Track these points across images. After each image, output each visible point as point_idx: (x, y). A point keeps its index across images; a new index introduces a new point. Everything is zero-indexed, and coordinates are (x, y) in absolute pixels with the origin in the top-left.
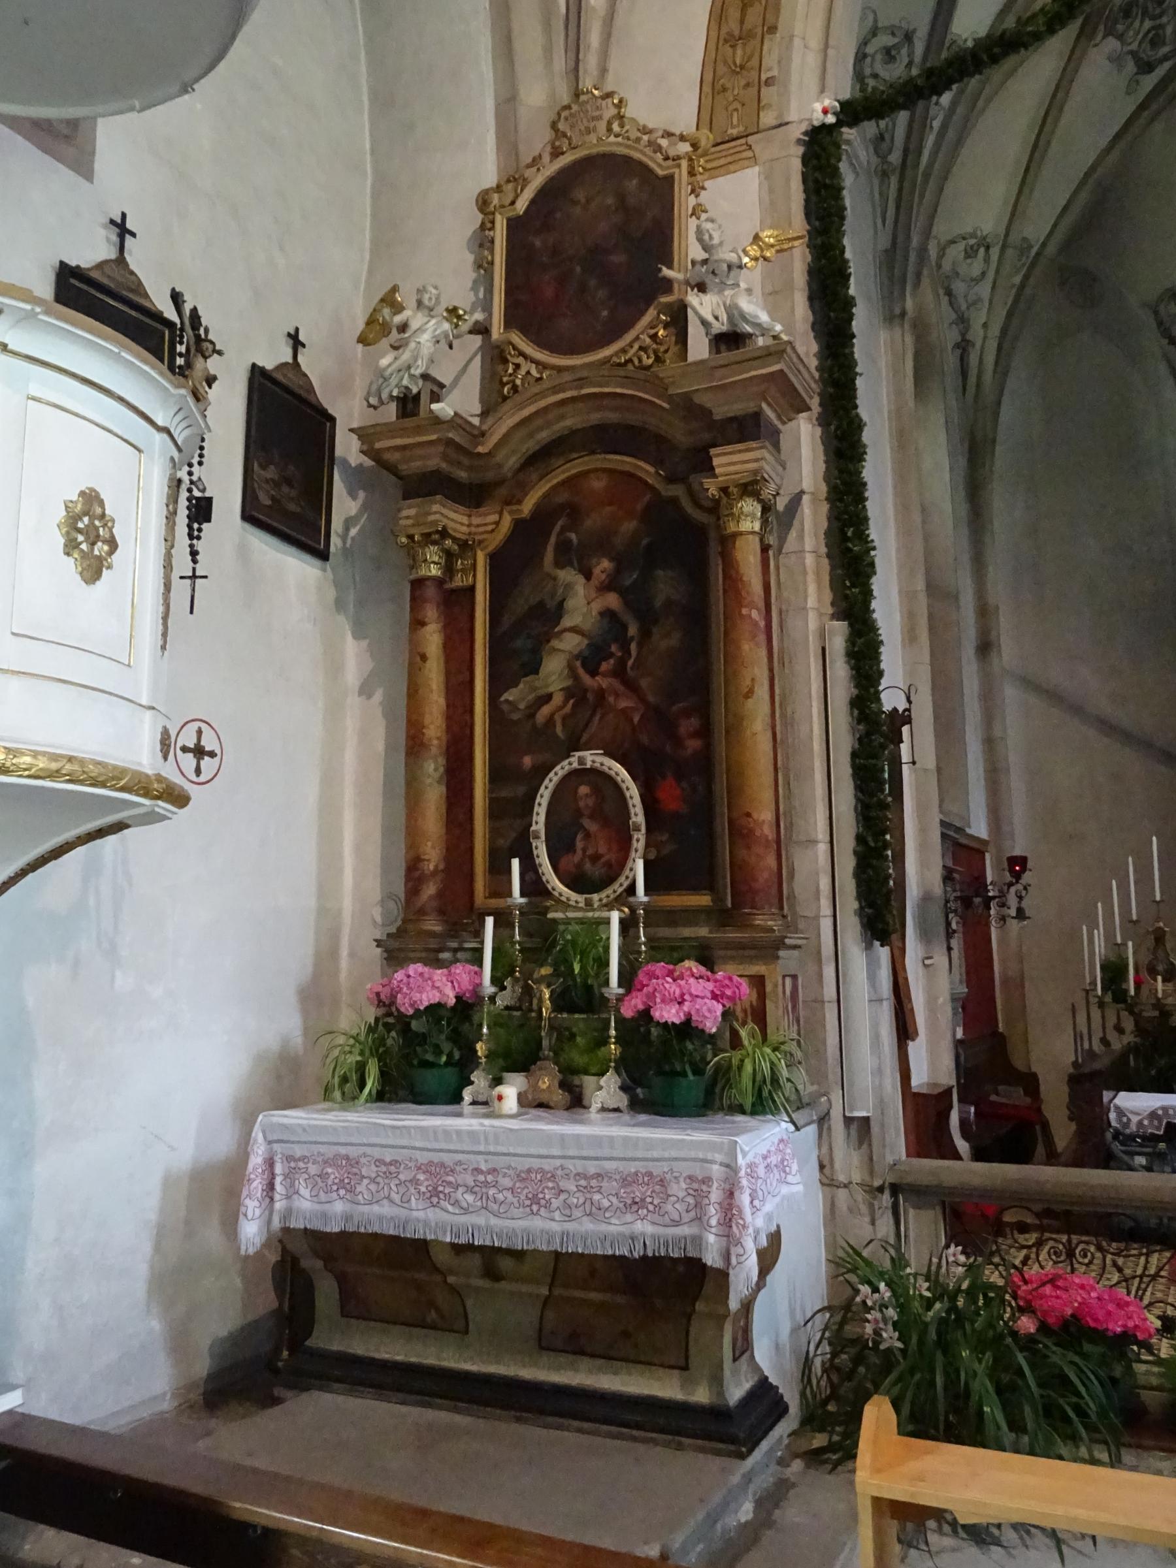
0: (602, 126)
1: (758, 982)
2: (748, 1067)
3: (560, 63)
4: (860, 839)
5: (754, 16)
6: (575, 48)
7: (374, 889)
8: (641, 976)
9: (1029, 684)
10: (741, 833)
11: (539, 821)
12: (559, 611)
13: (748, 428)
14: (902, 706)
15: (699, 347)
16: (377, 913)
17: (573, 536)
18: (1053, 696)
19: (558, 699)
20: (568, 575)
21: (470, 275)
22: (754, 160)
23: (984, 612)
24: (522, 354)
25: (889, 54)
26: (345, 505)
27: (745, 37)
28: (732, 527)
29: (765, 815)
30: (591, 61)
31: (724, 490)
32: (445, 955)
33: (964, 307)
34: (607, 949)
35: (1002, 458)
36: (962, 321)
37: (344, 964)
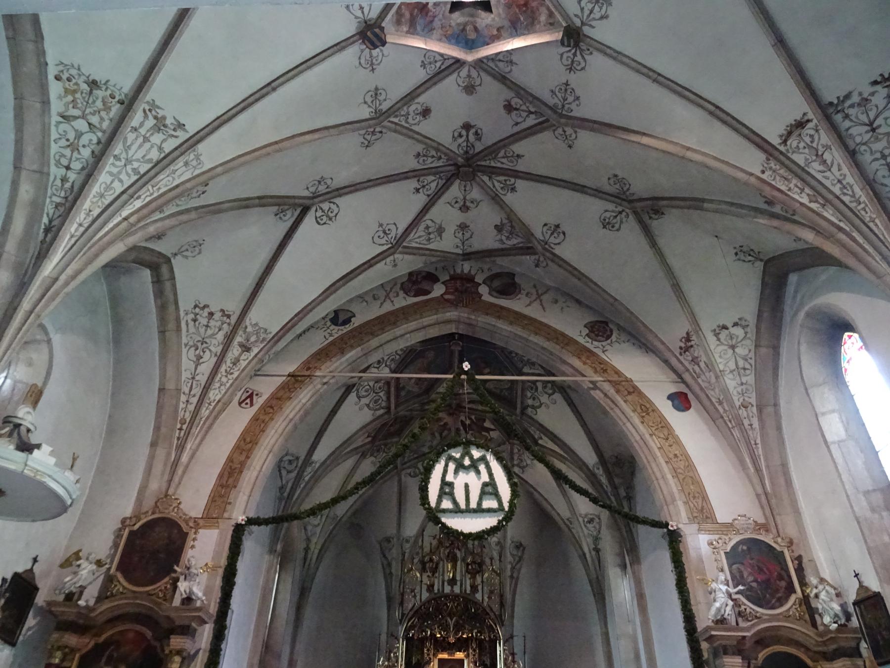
0: (171, 508)
3: (166, 477)
5: (231, 481)
13: (187, 631)
15: (177, 602)
17: (115, 655)
21: (110, 543)
22: (218, 527)
24: (119, 581)
25: (290, 462)
26: (31, 621)
30: (173, 485)
33: (310, 534)
36: (308, 540)
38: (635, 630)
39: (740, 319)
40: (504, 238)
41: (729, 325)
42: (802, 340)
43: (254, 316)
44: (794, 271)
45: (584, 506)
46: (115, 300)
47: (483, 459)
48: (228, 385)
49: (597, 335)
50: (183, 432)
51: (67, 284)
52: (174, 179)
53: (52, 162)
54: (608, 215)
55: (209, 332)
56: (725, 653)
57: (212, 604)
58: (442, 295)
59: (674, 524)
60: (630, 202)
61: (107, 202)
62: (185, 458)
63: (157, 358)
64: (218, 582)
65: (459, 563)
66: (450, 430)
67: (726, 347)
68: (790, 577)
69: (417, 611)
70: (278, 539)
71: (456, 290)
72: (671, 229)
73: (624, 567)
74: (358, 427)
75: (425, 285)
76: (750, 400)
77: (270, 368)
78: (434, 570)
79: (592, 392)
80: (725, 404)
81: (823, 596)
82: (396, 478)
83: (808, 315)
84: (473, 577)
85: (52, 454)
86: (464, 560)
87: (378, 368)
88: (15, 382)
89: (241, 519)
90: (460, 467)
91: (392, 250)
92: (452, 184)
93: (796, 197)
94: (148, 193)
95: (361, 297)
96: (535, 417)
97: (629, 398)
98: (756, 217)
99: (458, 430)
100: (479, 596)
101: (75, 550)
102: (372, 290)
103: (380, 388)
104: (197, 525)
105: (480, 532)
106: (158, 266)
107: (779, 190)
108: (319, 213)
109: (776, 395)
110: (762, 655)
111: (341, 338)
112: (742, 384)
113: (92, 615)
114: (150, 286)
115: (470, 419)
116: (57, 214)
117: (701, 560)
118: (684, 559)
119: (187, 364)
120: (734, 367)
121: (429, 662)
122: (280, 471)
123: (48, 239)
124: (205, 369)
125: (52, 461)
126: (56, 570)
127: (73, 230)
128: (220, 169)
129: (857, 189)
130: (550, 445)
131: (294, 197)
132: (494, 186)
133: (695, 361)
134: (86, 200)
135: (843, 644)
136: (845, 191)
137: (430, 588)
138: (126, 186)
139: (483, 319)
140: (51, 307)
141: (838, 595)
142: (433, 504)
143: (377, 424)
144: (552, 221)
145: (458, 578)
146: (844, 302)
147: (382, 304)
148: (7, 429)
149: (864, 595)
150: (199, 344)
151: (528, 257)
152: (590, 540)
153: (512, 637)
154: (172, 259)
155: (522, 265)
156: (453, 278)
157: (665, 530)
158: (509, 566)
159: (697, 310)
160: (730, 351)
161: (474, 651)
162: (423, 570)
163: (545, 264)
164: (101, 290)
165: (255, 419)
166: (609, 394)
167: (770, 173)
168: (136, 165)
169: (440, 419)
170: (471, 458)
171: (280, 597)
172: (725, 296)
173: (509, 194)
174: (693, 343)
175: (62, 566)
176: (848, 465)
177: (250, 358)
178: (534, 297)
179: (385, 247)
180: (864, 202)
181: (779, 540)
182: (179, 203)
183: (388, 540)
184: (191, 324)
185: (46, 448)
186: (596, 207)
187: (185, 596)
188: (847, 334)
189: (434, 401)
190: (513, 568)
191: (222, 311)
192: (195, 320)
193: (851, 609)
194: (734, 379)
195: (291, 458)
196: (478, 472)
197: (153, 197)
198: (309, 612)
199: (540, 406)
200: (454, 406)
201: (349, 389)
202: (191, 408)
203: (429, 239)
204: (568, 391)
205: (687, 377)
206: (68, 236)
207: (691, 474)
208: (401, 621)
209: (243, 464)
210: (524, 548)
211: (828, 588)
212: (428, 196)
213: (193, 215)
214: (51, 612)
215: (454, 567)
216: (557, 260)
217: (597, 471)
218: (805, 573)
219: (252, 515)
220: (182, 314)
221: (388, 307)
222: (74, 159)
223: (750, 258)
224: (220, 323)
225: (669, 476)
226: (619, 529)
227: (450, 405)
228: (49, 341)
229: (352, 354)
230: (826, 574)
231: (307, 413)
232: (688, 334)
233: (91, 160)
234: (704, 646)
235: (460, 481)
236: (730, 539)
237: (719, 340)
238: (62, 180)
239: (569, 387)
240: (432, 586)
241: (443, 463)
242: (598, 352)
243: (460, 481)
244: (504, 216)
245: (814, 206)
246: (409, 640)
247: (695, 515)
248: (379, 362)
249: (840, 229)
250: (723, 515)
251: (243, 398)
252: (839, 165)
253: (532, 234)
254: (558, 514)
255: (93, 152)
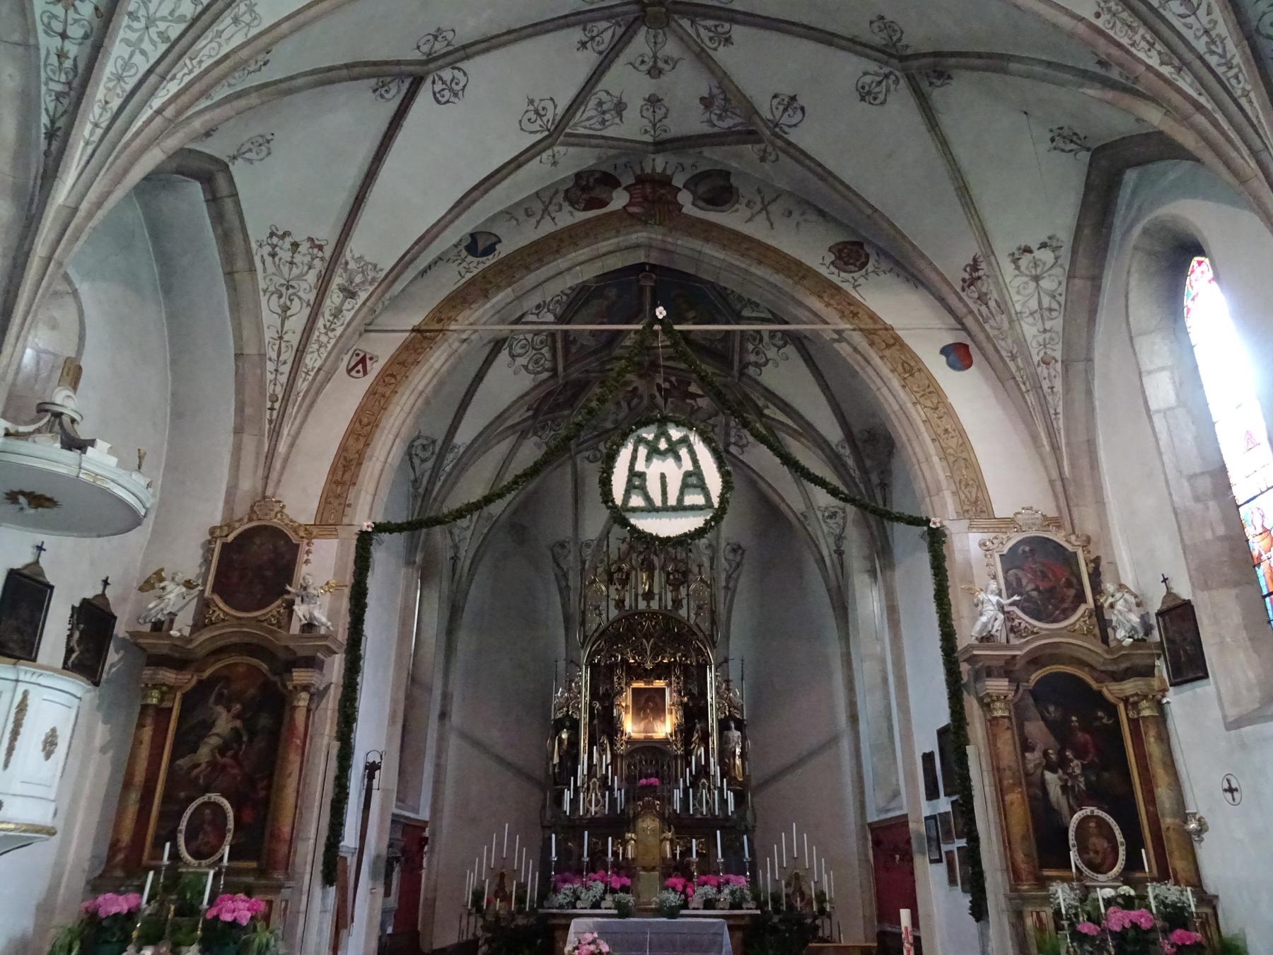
0: (273, 514)
1: (270, 903)
2: (257, 941)
3: (260, 472)
4: (328, 838)
5: (347, 476)
6: (269, 468)
7: (87, 852)
8: (218, 900)
9: (463, 735)
10: (275, 836)
11: (183, 825)
12: (213, 724)
13: (311, 663)
14: (378, 760)
15: (295, 628)
16: (86, 865)
17: (225, 691)
18: (476, 744)
19: (204, 766)
20: (220, 709)
21: (200, 560)
22: (337, 536)
23: (446, 696)
25: (424, 447)
26: (113, 656)
27: (342, 483)
28: (295, 703)
29: (286, 829)
31: (295, 687)
32: (123, 889)
34: (205, 886)
35: (467, 617)
37: (62, 891)
38: (883, 649)
39: (1050, 238)
40: (714, 117)
41: (1034, 247)
42: (1133, 269)
43: (357, 246)
44: (1129, 166)
45: (822, 498)
46: (157, 231)
47: (684, 441)
48: (330, 346)
49: (846, 263)
50: (275, 413)
51: (90, 215)
52: (220, 45)
53: (40, 28)
54: (868, 79)
55: (295, 271)
56: (989, 675)
57: (341, 630)
58: (624, 207)
59: (938, 520)
60: (903, 59)
61: (128, 88)
62: (282, 448)
63: (227, 313)
64: (345, 604)
65: (657, 572)
66: (641, 397)
67: (1026, 279)
68: (1081, 584)
69: (603, 633)
70: (416, 548)
71: (645, 198)
72: (961, 100)
73: (872, 573)
74: (514, 398)
75: (599, 192)
76: (1054, 354)
77: (386, 320)
78: (624, 582)
79: (836, 345)
80: (1019, 360)
81: (1120, 606)
82: (569, 469)
83: (1145, 231)
84: (676, 589)
85: (112, 451)
86: (663, 568)
87: (537, 315)
88: (39, 352)
89: (366, 525)
90: (654, 451)
91: (550, 140)
92: (635, 32)
93: (1141, 55)
94: (186, 71)
95: (508, 213)
96: (759, 378)
97: (887, 353)
98: (1081, 86)
99: (652, 397)
100: (683, 612)
101: (156, 569)
102: (522, 201)
103: (541, 342)
104: (309, 533)
105: (681, 536)
106: (209, 174)
107: (1120, 46)
108: (439, 86)
109: (1090, 347)
110: (1035, 677)
111: (484, 275)
112: (1045, 331)
113: (190, 647)
114: (204, 206)
115: (671, 382)
116: (61, 109)
117: (969, 565)
118: (947, 565)
119: (269, 318)
120: (1036, 307)
121: (620, 693)
122: (411, 459)
123: (53, 148)
124: (296, 323)
125: (113, 461)
126: (134, 594)
127: (86, 133)
128: (285, 27)
129: (1230, 45)
130: (781, 417)
131: (398, 63)
132: (698, 35)
133: (982, 298)
134: (97, 85)
135: (1138, 661)
136: (1213, 47)
137: (620, 604)
138: (152, 61)
139: (685, 244)
140: (76, 248)
141: (1138, 605)
142: (619, 501)
143: (541, 393)
144: (787, 91)
145: (656, 590)
146: (1194, 213)
147: (538, 222)
148: (46, 420)
149: (1171, 604)
150: (283, 290)
151: (749, 146)
152: (831, 540)
153: (726, 661)
154: (230, 165)
155: (740, 160)
156: (641, 180)
157: (925, 528)
158: (723, 576)
159: (990, 225)
160: (1032, 285)
161: (678, 678)
162: (610, 581)
163: (773, 157)
164: (135, 214)
165: (372, 392)
166: (859, 348)
167: (1108, 17)
168: (162, 26)
169: (627, 384)
170: (669, 439)
171: (425, 619)
172: (1032, 202)
173: (721, 48)
174: (981, 273)
175: (141, 589)
176: (1172, 441)
177: (357, 307)
178: (759, 206)
179: (539, 136)
180: (1238, 65)
181: (1073, 538)
182: (232, 81)
183: (562, 545)
184: (269, 260)
185: (102, 445)
186: (850, 69)
187: (304, 622)
188: (1197, 259)
189: (619, 359)
190: (729, 577)
191: (311, 239)
192: (273, 255)
193: (1153, 621)
194: (1034, 325)
195: (425, 442)
196: (678, 458)
197: (192, 76)
198: (465, 641)
199: (766, 364)
200: (646, 364)
201: (498, 345)
202: (283, 379)
203: (603, 122)
204: (805, 342)
205: (969, 321)
206: (82, 144)
207: (964, 455)
208: (583, 644)
209: (361, 455)
210: (744, 551)
211: (1127, 596)
212: (600, 53)
213: (253, 99)
214: (137, 645)
215: (651, 577)
216: (792, 151)
217: (842, 451)
218: (1102, 577)
219: (379, 520)
220: (254, 246)
221: (547, 228)
222: (70, 21)
223: (1073, 146)
224: (309, 258)
225: (935, 459)
226: (869, 527)
227: (640, 364)
228: (75, 293)
229: (500, 298)
230: (1128, 579)
231: (441, 384)
232: (975, 260)
233: (97, 22)
234: (964, 667)
235: (654, 470)
236: (1009, 539)
237: (1018, 268)
238: (59, 56)
239: (806, 337)
240: (623, 601)
241: (630, 447)
242: (847, 287)
243: (654, 470)
244: (714, 83)
245: (1166, 70)
246: (594, 668)
247: (966, 508)
248: (538, 307)
249: (1199, 107)
250: (1002, 509)
251: (353, 364)
252: (1209, 6)
253: (757, 112)
254: (789, 506)
255: (96, 9)
